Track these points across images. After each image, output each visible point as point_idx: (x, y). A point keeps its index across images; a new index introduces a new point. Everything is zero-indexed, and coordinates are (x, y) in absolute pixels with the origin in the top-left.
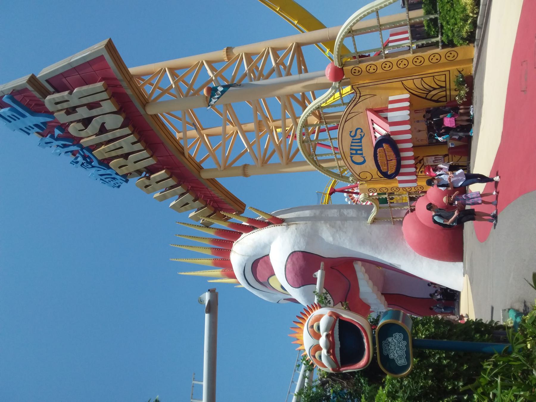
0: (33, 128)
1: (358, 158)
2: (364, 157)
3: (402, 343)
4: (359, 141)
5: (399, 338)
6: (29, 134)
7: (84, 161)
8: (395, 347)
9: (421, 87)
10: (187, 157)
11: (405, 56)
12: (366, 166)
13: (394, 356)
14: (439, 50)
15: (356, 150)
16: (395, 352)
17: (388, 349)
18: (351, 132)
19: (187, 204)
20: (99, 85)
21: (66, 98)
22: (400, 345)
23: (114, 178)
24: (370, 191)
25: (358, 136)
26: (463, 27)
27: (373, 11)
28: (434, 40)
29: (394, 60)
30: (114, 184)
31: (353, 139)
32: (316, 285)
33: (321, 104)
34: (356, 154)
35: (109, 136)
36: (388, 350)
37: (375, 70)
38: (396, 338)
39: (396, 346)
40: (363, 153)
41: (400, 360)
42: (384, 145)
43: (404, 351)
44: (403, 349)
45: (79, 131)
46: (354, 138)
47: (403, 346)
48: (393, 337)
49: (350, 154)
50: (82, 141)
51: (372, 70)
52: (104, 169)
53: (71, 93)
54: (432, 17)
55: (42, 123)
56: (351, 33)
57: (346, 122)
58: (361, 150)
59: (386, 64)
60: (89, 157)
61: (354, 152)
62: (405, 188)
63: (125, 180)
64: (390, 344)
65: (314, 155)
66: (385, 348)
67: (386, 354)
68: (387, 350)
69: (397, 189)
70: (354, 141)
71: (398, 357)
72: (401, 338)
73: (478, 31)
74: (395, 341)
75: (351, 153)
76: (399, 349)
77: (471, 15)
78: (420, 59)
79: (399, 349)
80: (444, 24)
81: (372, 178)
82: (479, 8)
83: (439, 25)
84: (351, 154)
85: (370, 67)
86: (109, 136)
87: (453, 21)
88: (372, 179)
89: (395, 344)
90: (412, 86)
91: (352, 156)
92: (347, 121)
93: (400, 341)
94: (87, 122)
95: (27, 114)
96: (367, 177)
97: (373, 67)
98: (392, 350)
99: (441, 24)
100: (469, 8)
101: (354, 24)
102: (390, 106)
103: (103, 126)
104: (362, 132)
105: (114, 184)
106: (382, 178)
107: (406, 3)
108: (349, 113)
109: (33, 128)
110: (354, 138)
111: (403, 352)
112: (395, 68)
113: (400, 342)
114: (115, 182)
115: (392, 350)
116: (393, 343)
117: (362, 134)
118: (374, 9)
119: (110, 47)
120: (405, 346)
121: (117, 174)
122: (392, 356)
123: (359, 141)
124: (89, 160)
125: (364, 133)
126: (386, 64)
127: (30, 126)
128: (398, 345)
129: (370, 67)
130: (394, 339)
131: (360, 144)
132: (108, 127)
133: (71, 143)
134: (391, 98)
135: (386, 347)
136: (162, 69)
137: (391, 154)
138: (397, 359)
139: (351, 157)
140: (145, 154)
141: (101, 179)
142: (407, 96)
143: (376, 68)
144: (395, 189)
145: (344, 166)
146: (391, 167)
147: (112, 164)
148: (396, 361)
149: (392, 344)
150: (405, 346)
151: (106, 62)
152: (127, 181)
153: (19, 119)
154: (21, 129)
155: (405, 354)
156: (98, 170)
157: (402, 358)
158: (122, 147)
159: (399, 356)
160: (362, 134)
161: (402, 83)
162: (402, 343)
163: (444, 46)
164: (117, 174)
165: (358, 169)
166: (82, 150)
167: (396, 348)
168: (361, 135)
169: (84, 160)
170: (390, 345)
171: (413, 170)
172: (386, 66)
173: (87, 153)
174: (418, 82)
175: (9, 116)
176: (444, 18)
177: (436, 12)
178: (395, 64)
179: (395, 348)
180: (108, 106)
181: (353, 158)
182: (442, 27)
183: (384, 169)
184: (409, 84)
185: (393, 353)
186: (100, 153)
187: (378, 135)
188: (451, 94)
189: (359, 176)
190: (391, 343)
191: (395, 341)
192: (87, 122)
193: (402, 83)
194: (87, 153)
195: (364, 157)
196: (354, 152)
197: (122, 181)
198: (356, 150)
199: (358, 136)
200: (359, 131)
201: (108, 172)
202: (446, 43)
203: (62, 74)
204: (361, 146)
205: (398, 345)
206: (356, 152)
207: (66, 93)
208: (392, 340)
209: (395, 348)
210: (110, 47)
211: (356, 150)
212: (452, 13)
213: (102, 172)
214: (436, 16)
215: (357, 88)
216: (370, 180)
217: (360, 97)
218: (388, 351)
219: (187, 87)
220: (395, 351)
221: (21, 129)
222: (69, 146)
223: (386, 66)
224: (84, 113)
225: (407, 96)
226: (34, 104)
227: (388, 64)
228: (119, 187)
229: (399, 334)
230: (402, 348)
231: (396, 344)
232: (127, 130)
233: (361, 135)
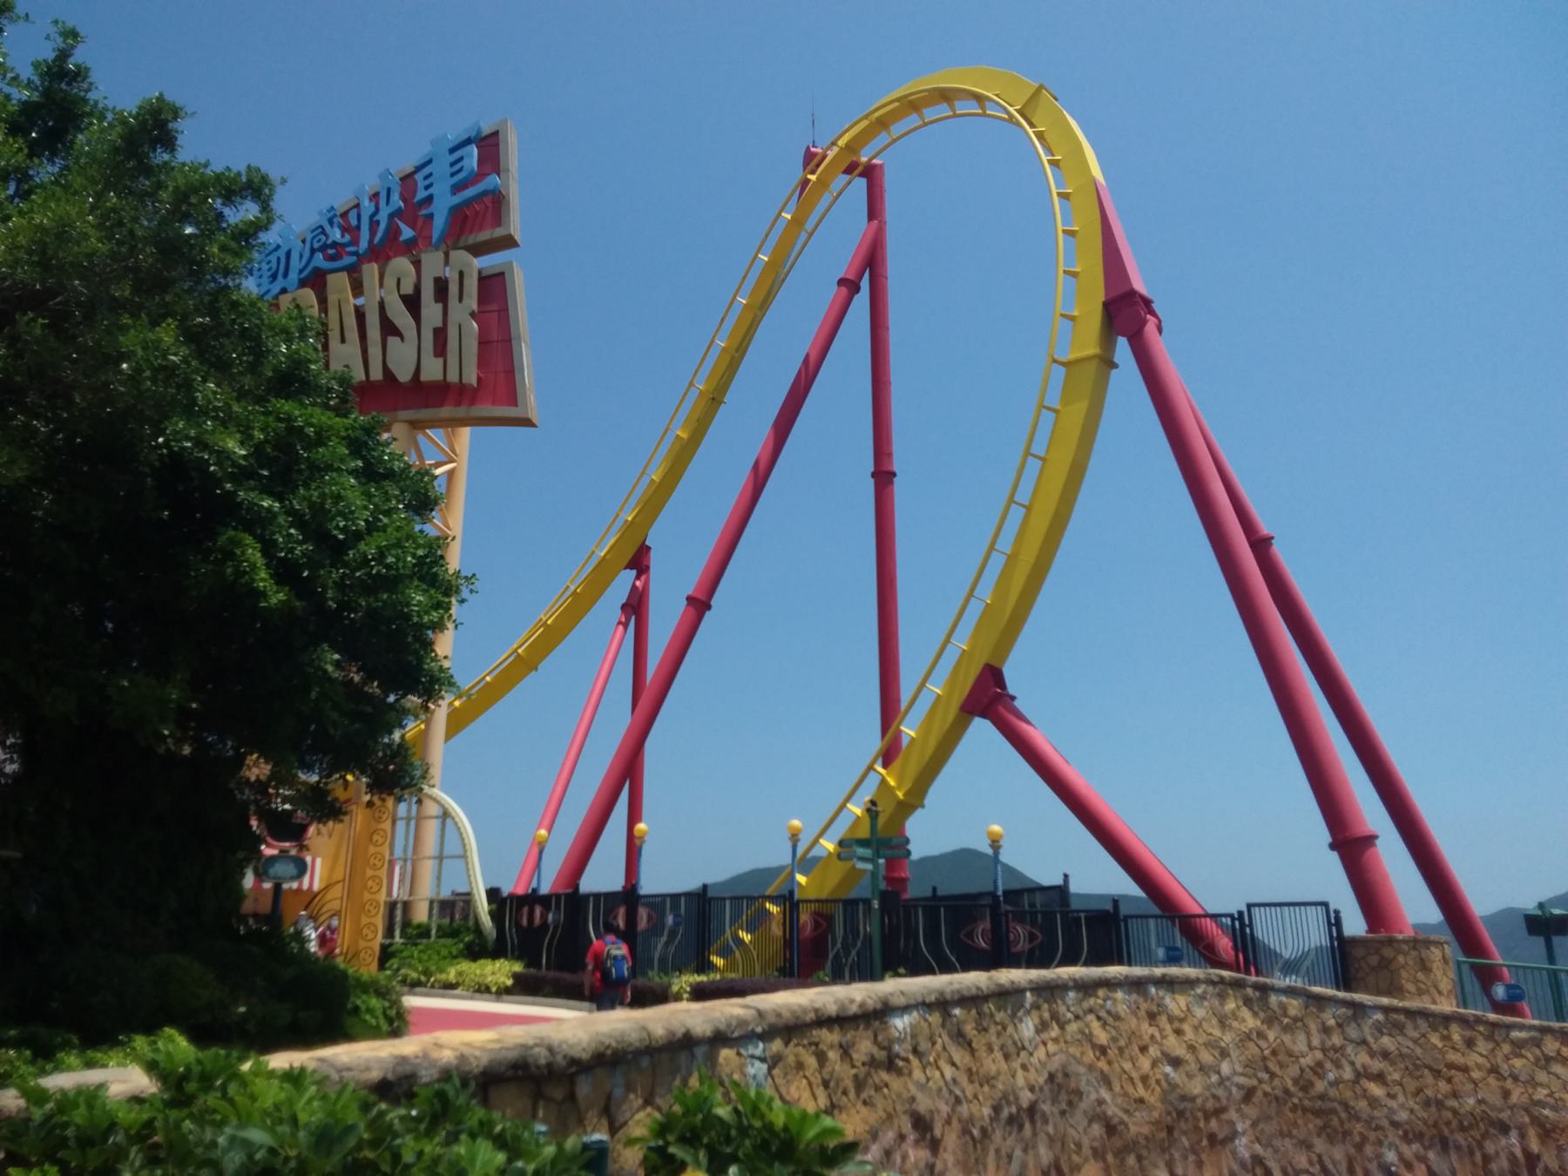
7: (329, 241)
9: (325, 909)
11: (384, 890)
14: (379, 939)
20: (471, 377)
21: (466, 300)
23: (274, 277)
26: (416, 970)
27: (465, 851)
28: (397, 933)
29: (383, 873)
35: (374, 332)
45: (399, 280)
51: (375, 837)
52: (301, 271)
53: (473, 315)
54: (433, 932)
55: (431, 216)
56: (446, 815)
73: (906, 727)
77: (432, 979)
78: (374, 912)
80: (421, 947)
82: (440, 988)
83: (419, 941)
86: (374, 332)
87: (426, 957)
90: (330, 896)
94: (413, 303)
95: (457, 199)
99: (421, 944)
100: (443, 977)
101: (456, 824)
103: (397, 332)
107: (457, 898)
112: (369, 873)
118: (468, 853)
119: (527, 422)
121: (284, 291)
132: (393, 341)
133: (381, 239)
136: (456, 455)
141: (278, 247)
142: (316, 887)
151: (502, 404)
153: (453, 175)
154: (430, 161)
156: (301, 256)
161: (338, 882)
163: (384, 948)
164: (284, 291)
166: (356, 253)
174: (335, 905)
175: (461, 159)
176: (428, 947)
177: (439, 937)
178: (377, 873)
180: (432, 370)
182: (416, 945)
184: (336, 892)
192: (413, 303)
193: (338, 882)
194: (348, 260)
201: (294, 276)
202: (390, 950)
203: (506, 310)
207: (475, 307)
210: (527, 422)
212: (436, 957)
213: (296, 264)
214: (433, 938)
221: (430, 161)
222: (373, 232)
226: (468, 213)
227: (379, 865)
232: (377, 374)
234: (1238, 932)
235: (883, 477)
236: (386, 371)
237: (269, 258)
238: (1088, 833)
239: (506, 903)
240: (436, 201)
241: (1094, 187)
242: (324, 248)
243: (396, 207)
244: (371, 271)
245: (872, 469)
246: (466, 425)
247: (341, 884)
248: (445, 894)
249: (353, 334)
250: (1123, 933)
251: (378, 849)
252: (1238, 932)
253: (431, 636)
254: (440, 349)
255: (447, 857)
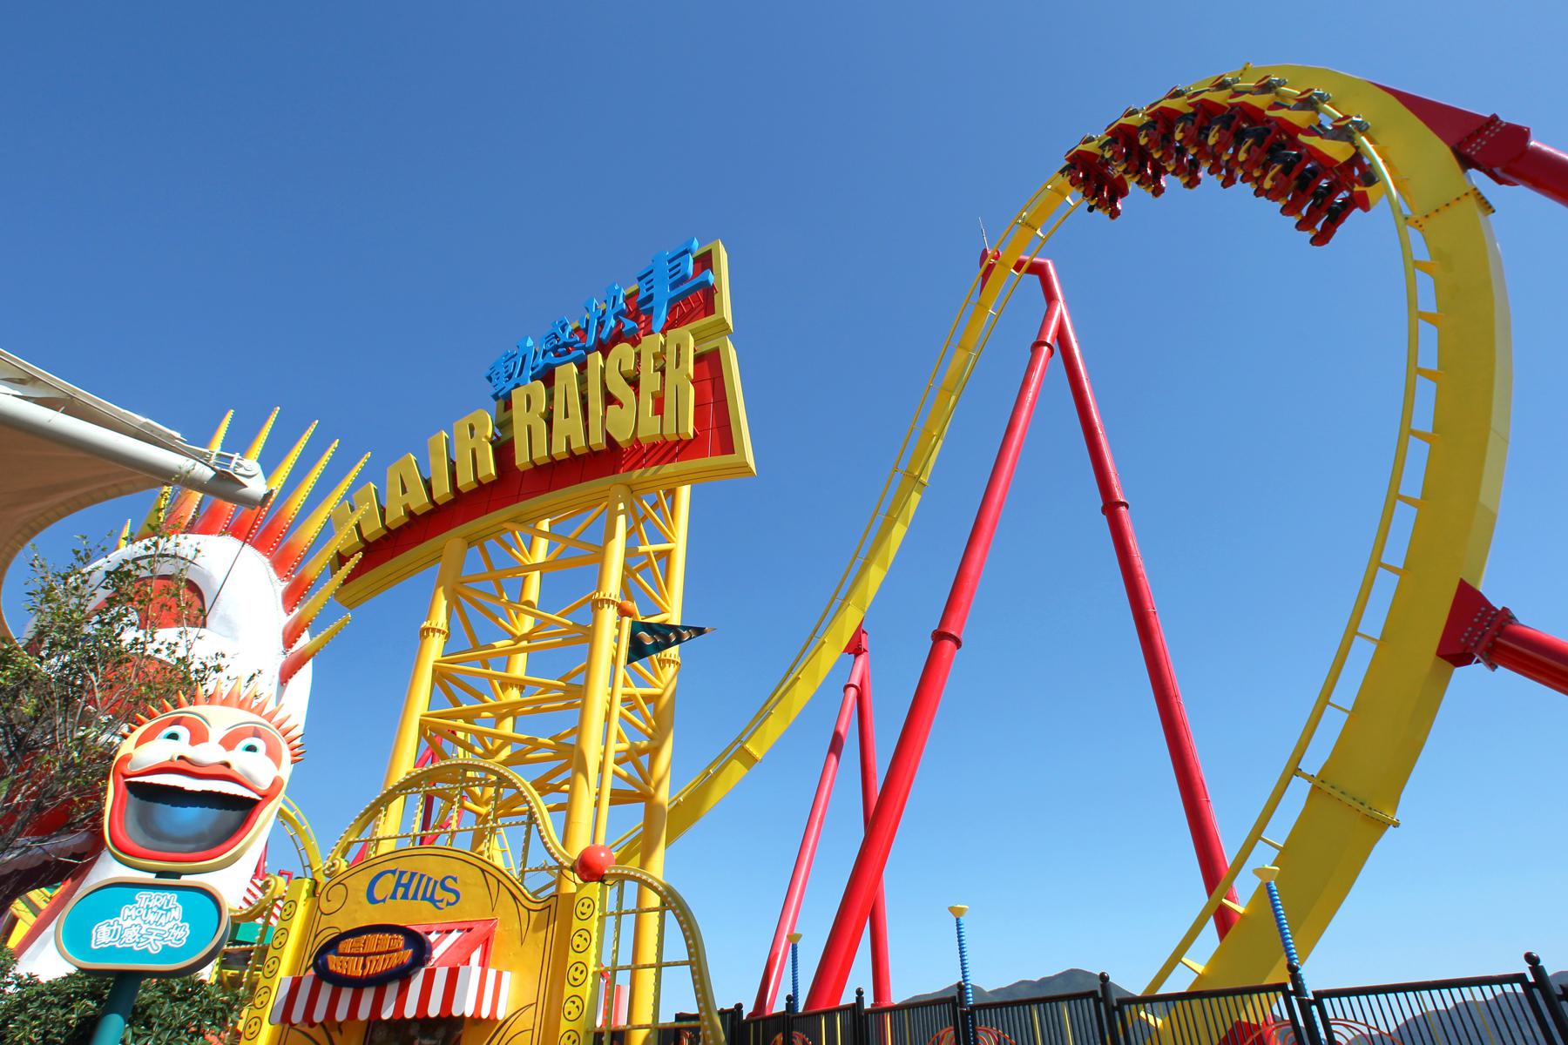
0: (647, 290)
1: (386, 886)
2: (384, 900)
3: (158, 943)
4: (428, 895)
5: (173, 936)
6: (640, 279)
7: (561, 342)
8: (152, 922)
10: (505, 525)
12: (360, 903)
13: (125, 918)
15: (407, 886)
16: (138, 921)
17: (147, 903)
18: (455, 880)
19: (404, 491)
22: (153, 937)
24: (288, 904)
25: (440, 894)
30: (498, 373)
31: (436, 882)
32: (612, 790)
33: (538, 826)
34: (398, 884)
35: (596, 404)
36: (148, 905)
37: (575, 948)
38: (177, 929)
39: (153, 926)
40: (407, 901)
41: (112, 931)
42: (410, 951)
43: (135, 944)
44: (138, 943)
46: (438, 886)
47: (150, 943)
48: (182, 921)
49: (403, 870)
50: (600, 355)
57: (483, 871)
58: (405, 896)
59: (582, 972)
60: (569, 352)
61: (405, 880)
62: (266, 992)
63: (500, 394)
64: (164, 912)
65: (464, 784)
66: (157, 897)
67: (137, 899)
68: (150, 901)
69: (271, 972)
70: (432, 883)
71: (120, 927)
72: (174, 941)
74: (171, 925)
75: (405, 872)
76: (143, 931)
79: (143, 931)
81: (322, 913)
84: (402, 873)
85: (585, 939)
86: (596, 404)
88: (319, 913)
89: (161, 924)
91: (398, 873)
92: (484, 874)
93: (163, 939)
95: (674, 293)
96: (329, 901)
97: (583, 945)
98: (146, 916)
102: (491, 973)
104: (448, 904)
105: (498, 373)
106: (316, 936)
108: (499, 881)
109: (647, 290)
110: (438, 886)
111: (132, 941)
113: (161, 938)
114: (503, 375)
115: (146, 916)
116: (163, 920)
117: (443, 905)
120: (147, 948)
121: (517, 386)
122: (128, 913)
123: (428, 895)
124: (560, 350)
125: (442, 909)
126: (582, 972)
127: (652, 287)
128: (156, 932)
129: (585, 939)
130: (174, 922)
131: (420, 895)
134: (506, 976)
135: (159, 899)
137: (378, 966)
138: (116, 923)
139: (393, 872)
140: (541, 453)
142: (501, 1015)
143: (580, 949)
144: (272, 967)
145: (375, 852)
146: (347, 963)
147: (540, 385)
148: (112, 921)
149: (164, 916)
150: (147, 948)
152: (496, 397)
154: (651, 272)
155: (125, 945)
157: (115, 936)
158: (567, 416)
159: (123, 930)
160: (443, 905)
162: (158, 943)
165: (360, 882)
166: (583, 348)
167: (148, 926)
168: (442, 901)
169: (565, 343)
170: (161, 912)
171: (319, 1015)
172: (579, 971)
173: (575, 354)
175: (679, 265)
179: (149, 922)
180: (650, 428)
181: (390, 875)
183: (346, 946)
185: (137, 916)
186: (567, 373)
187: (433, 937)
188: (1496, 994)
189: (339, 883)
190: (166, 914)
191: (171, 925)
194: (575, 354)
195: (384, 900)
196: (405, 880)
197: (499, 388)
198: (407, 887)
199: (440, 894)
200: (452, 897)
204: (415, 897)
205: (156, 932)
206: (403, 885)
208: (174, 918)
209: (149, 922)
211: (407, 886)
215: (550, 906)
216: (319, 907)
217: (529, 910)
218: (147, 903)
219: (634, 568)
220: (142, 923)
221: (651, 272)
222: (598, 332)
223: (579, 971)
224: (649, 381)
225: (501, 1015)
227: (581, 978)
228: (490, 379)
229: (184, 939)
230: (142, 940)
231: (159, 927)
233: (442, 901)
234: (1304, 1032)
235: (1111, 508)
236: (609, 439)
237: (507, 363)
238: (1194, 943)
239: (130, 782)
240: (655, 298)
241: (1373, 86)
242: (555, 349)
243: (620, 309)
244: (596, 359)
245: (1101, 504)
246: (684, 485)
247: (1353, 1019)
248: (667, 1018)
249: (576, 409)
250: (1121, 1036)
251: (580, 957)
252: (1304, 1032)
253: (621, 471)
254: (659, 409)
255: (668, 965)
